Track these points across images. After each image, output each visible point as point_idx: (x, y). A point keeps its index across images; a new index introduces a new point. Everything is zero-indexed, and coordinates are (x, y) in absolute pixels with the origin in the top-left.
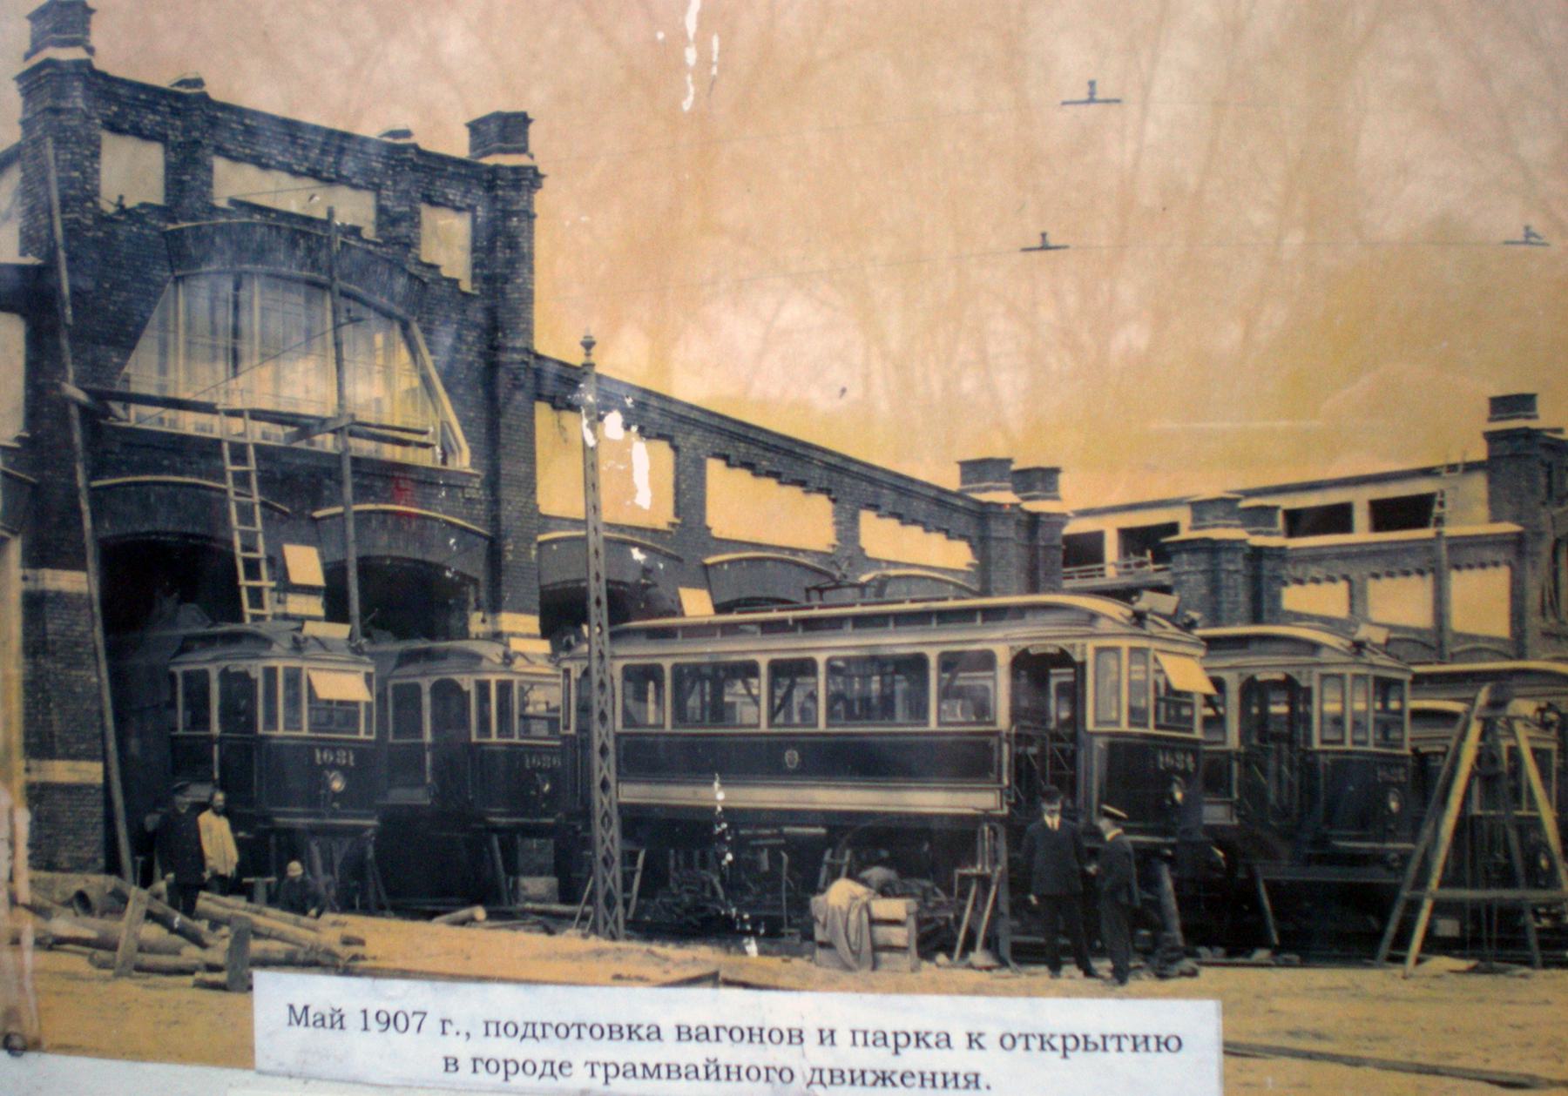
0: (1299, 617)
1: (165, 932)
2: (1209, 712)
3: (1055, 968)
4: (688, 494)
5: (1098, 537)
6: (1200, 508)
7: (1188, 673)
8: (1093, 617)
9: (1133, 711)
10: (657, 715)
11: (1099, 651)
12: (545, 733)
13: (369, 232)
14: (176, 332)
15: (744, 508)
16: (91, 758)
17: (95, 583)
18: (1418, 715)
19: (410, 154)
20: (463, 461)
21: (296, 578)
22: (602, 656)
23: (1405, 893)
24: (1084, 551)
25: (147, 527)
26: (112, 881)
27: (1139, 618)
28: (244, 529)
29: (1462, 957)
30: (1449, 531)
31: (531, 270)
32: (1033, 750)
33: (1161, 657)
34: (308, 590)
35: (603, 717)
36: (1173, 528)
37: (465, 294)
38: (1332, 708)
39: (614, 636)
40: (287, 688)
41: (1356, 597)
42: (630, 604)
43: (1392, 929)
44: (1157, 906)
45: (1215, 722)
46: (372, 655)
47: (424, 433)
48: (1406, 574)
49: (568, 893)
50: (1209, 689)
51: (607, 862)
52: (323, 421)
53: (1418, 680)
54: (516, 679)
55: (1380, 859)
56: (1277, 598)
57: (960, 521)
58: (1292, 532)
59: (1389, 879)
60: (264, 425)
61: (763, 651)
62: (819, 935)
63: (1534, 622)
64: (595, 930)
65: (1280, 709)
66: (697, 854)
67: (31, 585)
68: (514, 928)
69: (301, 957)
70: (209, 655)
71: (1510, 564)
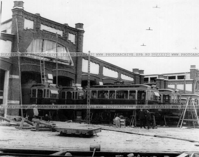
0: (169, 88)
1: (27, 123)
2: (159, 98)
3: (141, 127)
4: (101, 70)
5: (148, 78)
6: (159, 76)
7: (157, 94)
8: (147, 87)
9: (151, 98)
10: (95, 97)
11: (147, 91)
12: (81, 99)
13: (62, 36)
14: (34, 46)
15: (108, 73)
16: (18, 100)
17: (20, 77)
18: (182, 99)
19: (68, 27)
20: (73, 65)
21: (49, 78)
22: (89, 89)
23: (180, 119)
24: (146, 80)
25: (28, 70)
26: (20, 117)
27: (152, 88)
28: (42, 70)
29: (186, 127)
30: (186, 80)
31: (83, 42)
32: (139, 102)
33: (154, 92)
34: (51, 80)
35: (89, 97)
36: (156, 78)
37: (74, 44)
38: (173, 98)
39: (91, 87)
40: (47, 92)
41: (176, 86)
42: (93, 83)
43: (179, 123)
44: (153, 120)
45: (160, 99)
46: (59, 88)
47: (67, 61)
48: (181, 84)
49: (83, 118)
50: (159, 96)
51: (88, 115)
52: (54, 59)
53: (182, 96)
54: (78, 92)
55: (178, 116)
56: (167, 86)
57: (132, 76)
58: (169, 79)
59: (178, 118)
60: (46, 58)
61: (109, 89)
62: (114, 123)
63: (195, 90)
64: (86, 123)
65: (167, 98)
66: (100, 114)
67: (10, 77)
68: (76, 123)
69: (47, 127)
70: (36, 87)
71: (192, 83)
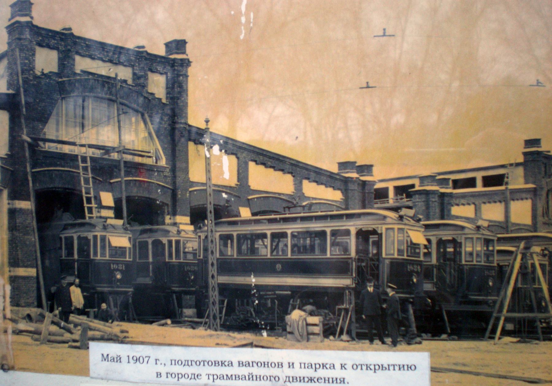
0: (457, 217)
1: (58, 328)
2: (426, 251)
3: (372, 341)
4: (242, 174)
5: (387, 189)
6: (423, 179)
7: (418, 237)
8: (385, 217)
9: (399, 250)
10: (231, 252)
11: (387, 229)
12: (192, 258)
13: (130, 82)
14: (62, 117)
15: (262, 179)
16: (32, 267)
17: (33, 205)
18: (499, 252)
19: (145, 54)
20: (163, 162)
21: (104, 204)
22: (212, 231)
23: (495, 315)
24: (382, 194)
25: (52, 186)
26: (39, 310)
27: (401, 218)
28: (86, 186)
29: (515, 337)
30: (510, 187)
31: (187, 95)
32: (364, 264)
33: (409, 231)
34: (109, 208)
35: (212, 252)
36: (413, 186)
37: (164, 104)
38: (469, 249)
39: (216, 224)
40: (101, 242)
41: (477, 210)
42: (222, 213)
43: (490, 327)
44: (407, 319)
45: (428, 254)
46: (131, 231)
47: (149, 152)
48: (495, 202)
49: (200, 315)
50: (426, 243)
51: (214, 304)
52: (114, 148)
53: (499, 239)
54: (182, 239)
55: (486, 303)
56: (449, 210)
57: (338, 184)
58: (455, 187)
59: (489, 310)
60: (93, 150)
61: (269, 229)
62: (288, 329)
63: (540, 219)
64: (209, 327)
65: (451, 250)
66: (245, 301)
67: (11, 206)
68: (181, 327)
69: (106, 337)
70: (74, 231)
71: (531, 199)
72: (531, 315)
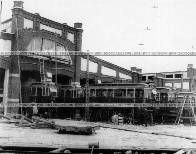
0: (167, 87)
1: (27, 121)
2: (157, 96)
3: (139, 125)
4: (99, 69)
5: (145, 77)
6: (157, 74)
7: (155, 92)
8: (145, 85)
9: (149, 96)
10: (94, 95)
11: (145, 89)
12: (80, 97)
13: (61, 35)
14: (34, 45)
15: (106, 71)
16: (18, 98)
17: (20, 75)
18: (179, 98)
19: (67, 26)
20: (72, 63)
21: (49, 76)
22: (88, 88)
23: (177, 117)
24: (144, 78)
25: (28, 69)
26: (19, 115)
27: (150, 86)
28: (42, 69)
29: (183, 124)
30: (183, 78)
31: (81, 42)
32: (137, 100)
33: (152, 90)
34: (50, 78)
35: (87, 95)
36: (154, 76)
37: (73, 44)
38: (170, 96)
39: (89, 85)
40: (46, 90)
41: (173, 85)
42: (92, 82)
43: (176, 121)
44: (151, 118)
45: (158, 98)
46: (58, 86)
47: (66, 60)
48: (178, 82)
49: (82, 116)
50: (157, 94)
51: (87, 112)
52: (53, 57)
53: (179, 94)
54: (77, 90)
55: (175, 113)
56: (165, 84)
57: (130, 74)
58: (167, 77)
59: (176, 115)
60: (45, 57)
61: (107, 88)
62: (112, 121)
63: (192, 88)
64: (85, 121)
65: (165, 96)
66: (98, 112)
67: (10, 76)
68: (75, 120)
69: (46, 124)
70: (36, 86)
71: (189, 82)
72: (114, 93)
